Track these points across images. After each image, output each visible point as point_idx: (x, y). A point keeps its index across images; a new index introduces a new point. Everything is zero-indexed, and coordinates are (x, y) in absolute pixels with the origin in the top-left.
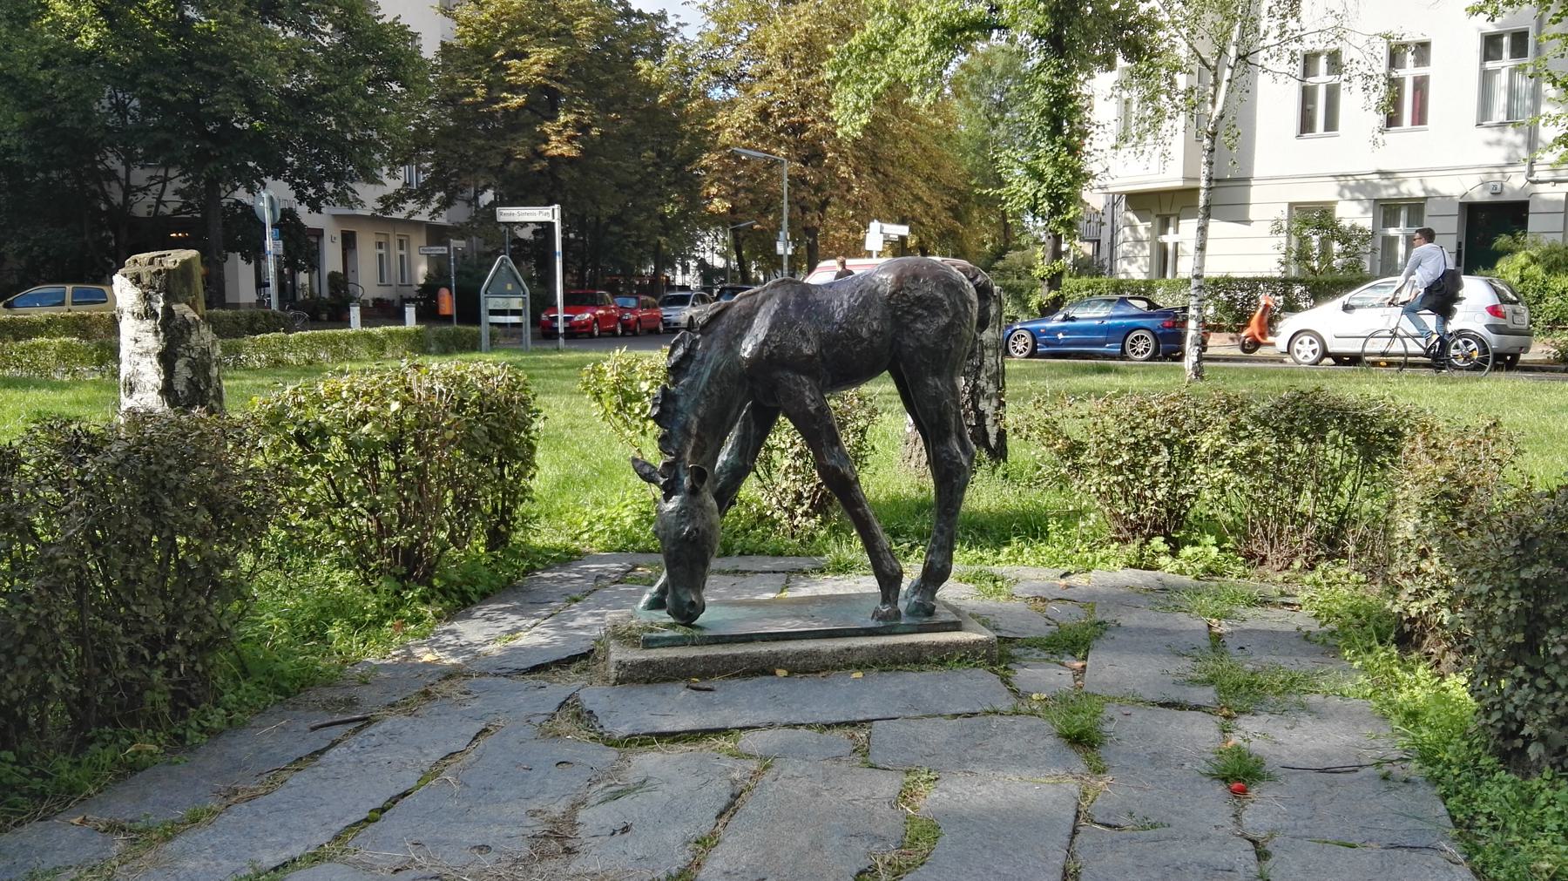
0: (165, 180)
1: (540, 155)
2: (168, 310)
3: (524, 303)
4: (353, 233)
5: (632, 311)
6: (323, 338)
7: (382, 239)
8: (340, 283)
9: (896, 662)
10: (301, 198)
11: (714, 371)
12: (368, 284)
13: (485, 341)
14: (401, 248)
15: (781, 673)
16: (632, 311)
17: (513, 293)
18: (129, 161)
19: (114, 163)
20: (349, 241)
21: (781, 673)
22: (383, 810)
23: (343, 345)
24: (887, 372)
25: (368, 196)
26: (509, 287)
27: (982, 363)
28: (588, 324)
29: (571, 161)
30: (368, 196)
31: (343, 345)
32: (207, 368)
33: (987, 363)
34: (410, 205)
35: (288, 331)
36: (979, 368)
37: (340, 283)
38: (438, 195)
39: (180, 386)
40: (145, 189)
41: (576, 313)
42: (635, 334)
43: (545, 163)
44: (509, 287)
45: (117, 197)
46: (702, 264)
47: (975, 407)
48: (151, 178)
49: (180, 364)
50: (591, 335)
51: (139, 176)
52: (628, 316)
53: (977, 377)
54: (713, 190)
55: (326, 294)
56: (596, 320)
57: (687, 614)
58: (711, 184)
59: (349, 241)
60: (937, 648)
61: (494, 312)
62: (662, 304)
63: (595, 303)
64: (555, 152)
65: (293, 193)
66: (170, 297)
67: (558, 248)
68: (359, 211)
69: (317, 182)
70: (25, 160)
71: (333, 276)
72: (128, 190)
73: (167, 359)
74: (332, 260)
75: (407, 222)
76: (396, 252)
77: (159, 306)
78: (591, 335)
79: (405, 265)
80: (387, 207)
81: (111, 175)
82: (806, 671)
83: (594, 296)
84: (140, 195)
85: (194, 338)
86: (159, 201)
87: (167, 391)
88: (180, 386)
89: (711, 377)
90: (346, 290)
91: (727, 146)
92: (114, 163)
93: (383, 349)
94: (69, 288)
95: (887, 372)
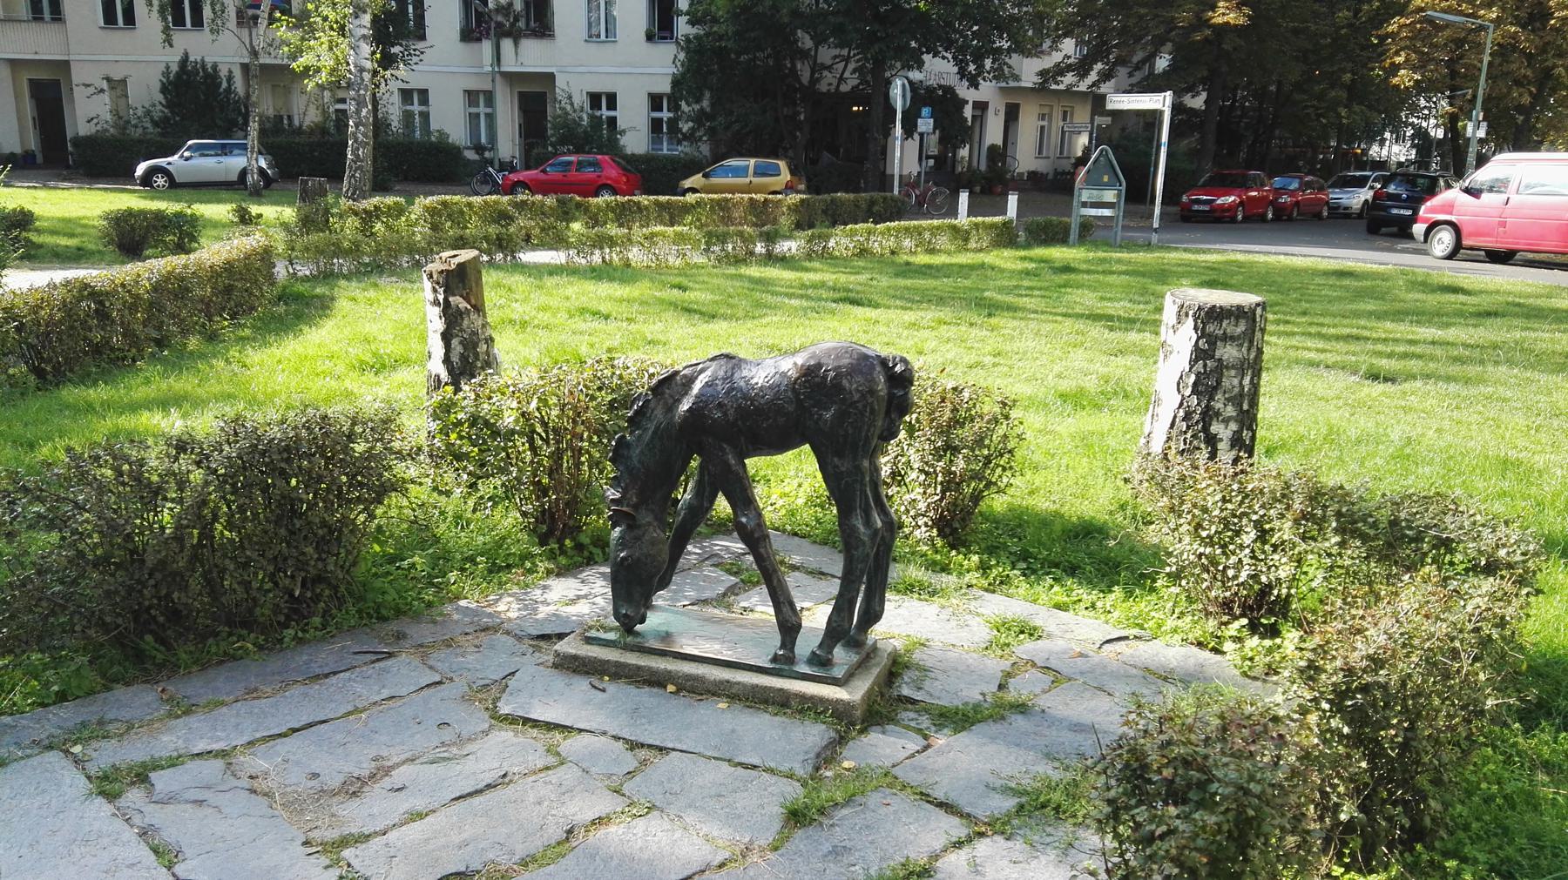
0: (847, 60)
1: (1206, 23)
2: (446, 299)
3: (1119, 196)
4: (1017, 106)
5: (1292, 193)
6: (907, 229)
7: (1046, 111)
8: (998, 155)
9: (766, 702)
10: (962, 73)
11: (657, 428)
12: (1025, 159)
13: (1074, 234)
14: (1064, 119)
15: (671, 688)
16: (1292, 193)
17: (1109, 186)
18: (819, 40)
19: (806, 42)
20: (1012, 114)
21: (671, 688)
22: (297, 730)
23: (927, 235)
24: (807, 446)
25: (1028, 70)
26: (1106, 179)
27: (1219, 382)
28: (1232, 208)
29: (1236, 29)
30: (1028, 70)
31: (927, 235)
32: (475, 345)
33: (1226, 383)
34: (1069, 78)
35: (876, 223)
36: (1215, 389)
37: (998, 155)
38: (1099, 66)
39: (455, 359)
40: (829, 68)
41: (1219, 196)
42: (1290, 219)
43: (1208, 32)
44: (1106, 179)
45: (805, 77)
46: (1421, 134)
47: (1206, 429)
48: (836, 57)
49: (455, 342)
50: (1233, 220)
51: (826, 54)
52: (1285, 199)
53: (1211, 398)
54: (1399, 59)
55: (983, 167)
56: (1242, 203)
57: (628, 624)
58: (1397, 53)
59: (1012, 114)
60: (803, 698)
61: (1084, 205)
62: (1333, 186)
63: (1240, 184)
64: (1220, 20)
65: (956, 69)
66: (448, 292)
67: (1165, 137)
68: (1023, 84)
69: (978, 59)
70: (730, 44)
71: (992, 148)
72: (817, 68)
73: (446, 337)
74: (993, 133)
75: (1068, 92)
76: (1058, 123)
77: (441, 298)
78: (1233, 220)
79: (1065, 138)
80: (1046, 81)
81: (804, 55)
82: (692, 691)
83: (1245, 176)
84: (825, 73)
85: (466, 322)
86: (841, 79)
87: (447, 361)
88: (455, 359)
89: (655, 433)
90: (1004, 163)
91: (1422, 10)
92: (806, 42)
93: (966, 240)
94: (752, 161)
95: (807, 446)
